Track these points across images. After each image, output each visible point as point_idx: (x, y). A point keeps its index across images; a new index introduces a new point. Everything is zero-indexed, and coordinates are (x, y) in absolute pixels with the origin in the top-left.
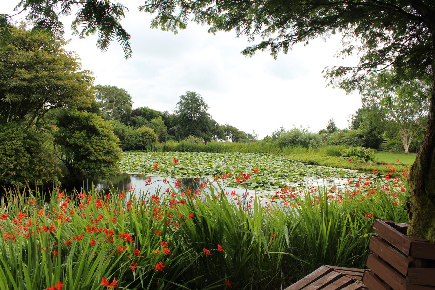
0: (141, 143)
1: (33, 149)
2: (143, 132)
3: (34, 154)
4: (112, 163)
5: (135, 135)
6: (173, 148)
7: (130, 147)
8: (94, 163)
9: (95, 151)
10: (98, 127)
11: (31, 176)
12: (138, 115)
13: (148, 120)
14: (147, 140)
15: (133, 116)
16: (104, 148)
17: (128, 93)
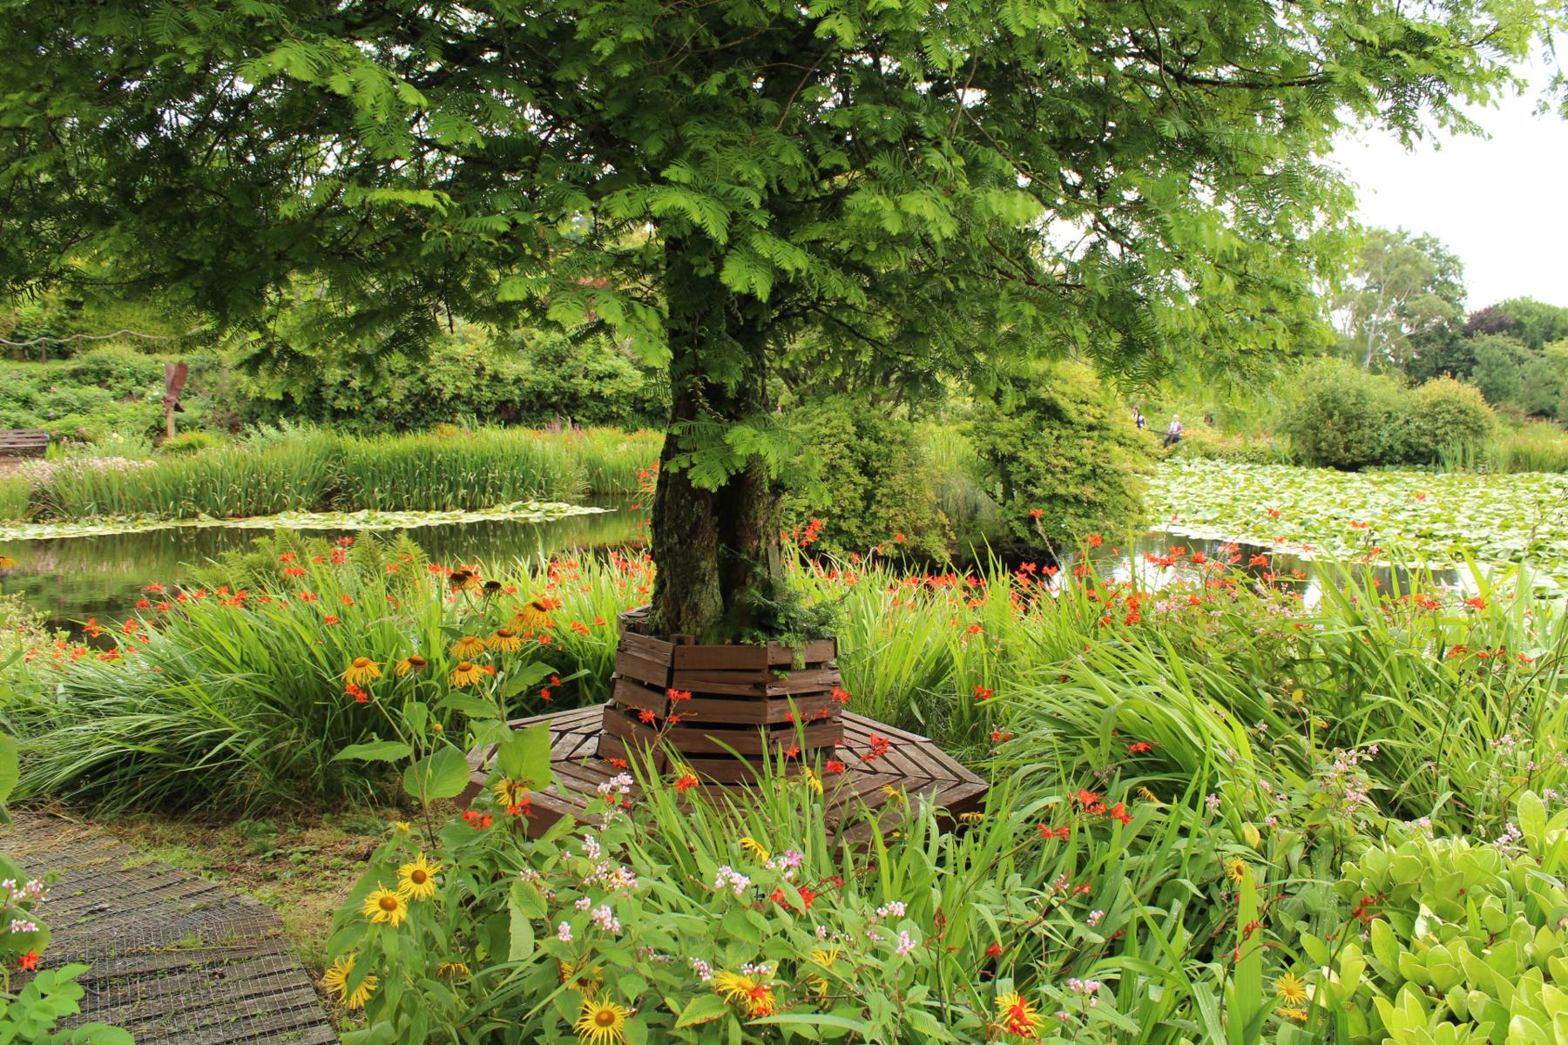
0: (1426, 440)
1: (876, 464)
2: (1435, 398)
3: (878, 478)
4: (1101, 505)
5: (1402, 411)
6: (1552, 461)
7: (1383, 455)
8: (1046, 505)
9: (1048, 471)
10: (1063, 403)
11: (868, 532)
12: (1491, 332)
13: (1533, 346)
14: (1449, 428)
15: (1468, 333)
16: (1081, 464)
17: (1451, 252)
